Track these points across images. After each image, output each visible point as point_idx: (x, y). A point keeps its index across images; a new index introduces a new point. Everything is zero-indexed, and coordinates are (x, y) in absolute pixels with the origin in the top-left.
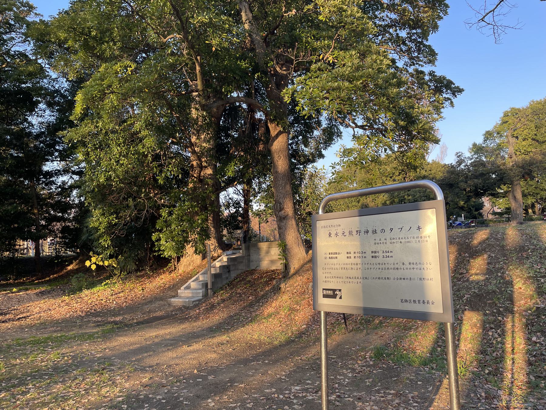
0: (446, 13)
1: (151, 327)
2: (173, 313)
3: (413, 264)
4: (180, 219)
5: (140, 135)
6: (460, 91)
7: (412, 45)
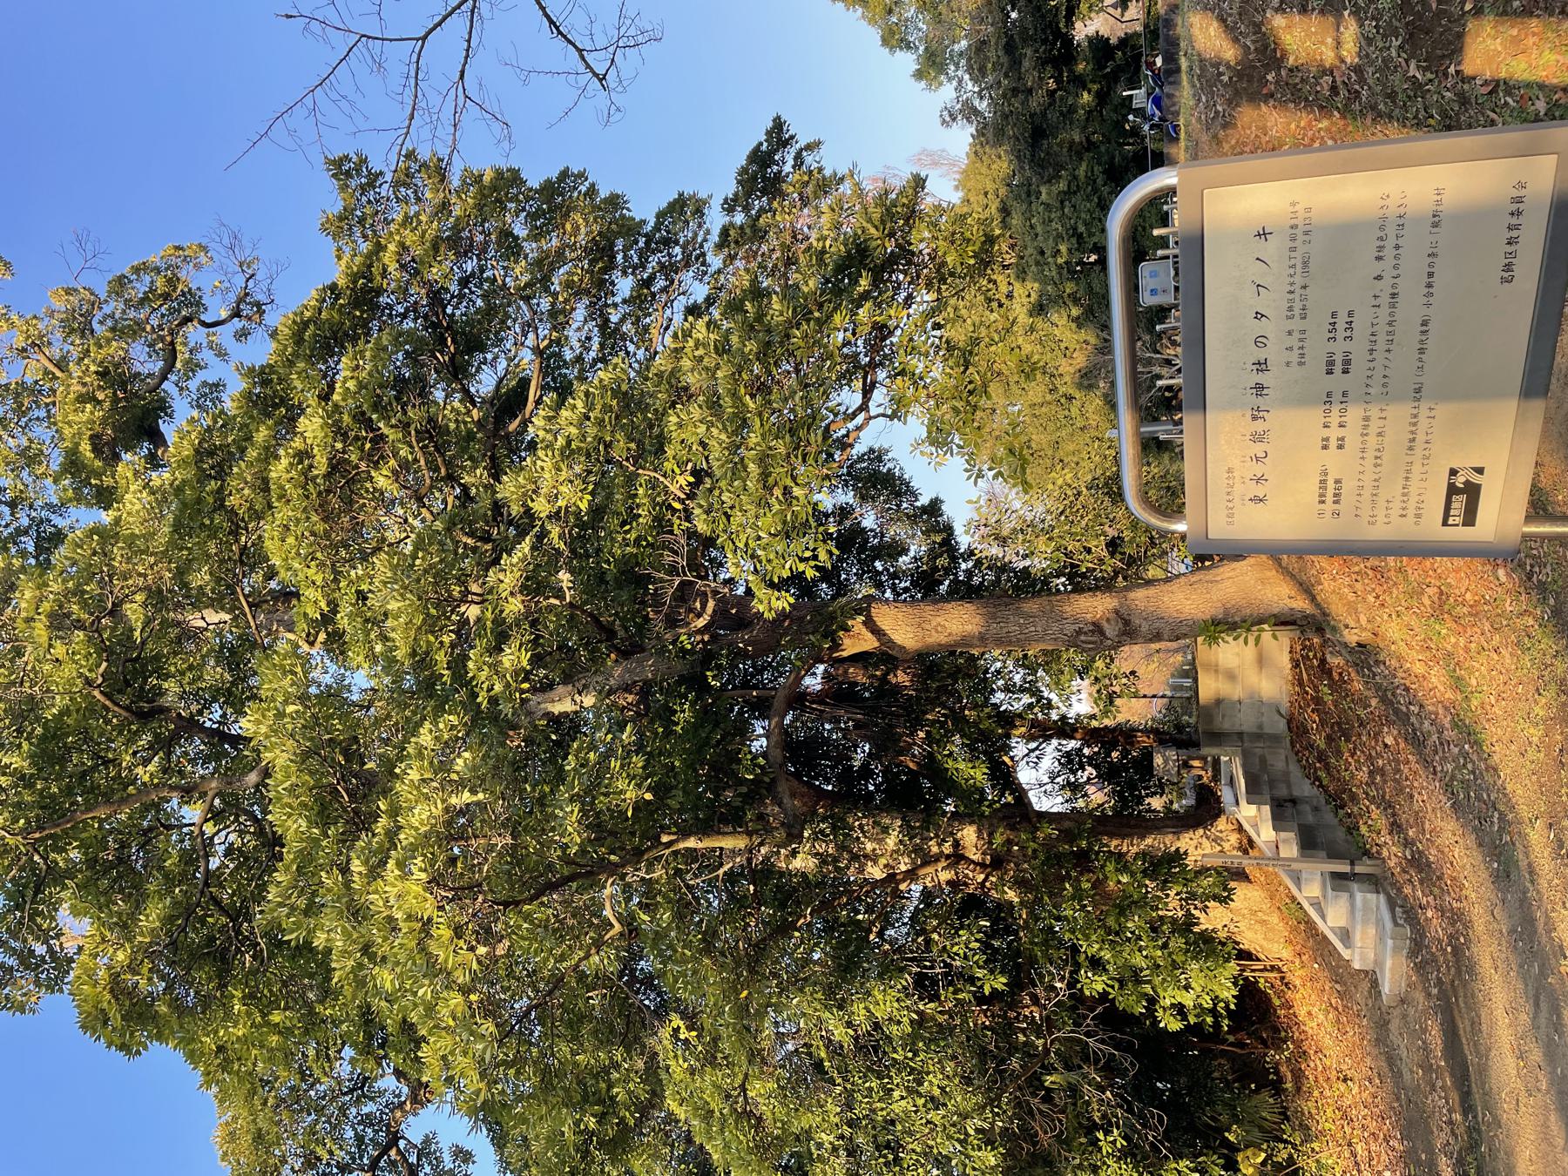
0: (582, 175)
1: (1483, 1070)
2: (1435, 991)
3: (1380, 248)
4: (1114, 936)
5: (866, 1027)
6: (778, 124)
7: (653, 262)
